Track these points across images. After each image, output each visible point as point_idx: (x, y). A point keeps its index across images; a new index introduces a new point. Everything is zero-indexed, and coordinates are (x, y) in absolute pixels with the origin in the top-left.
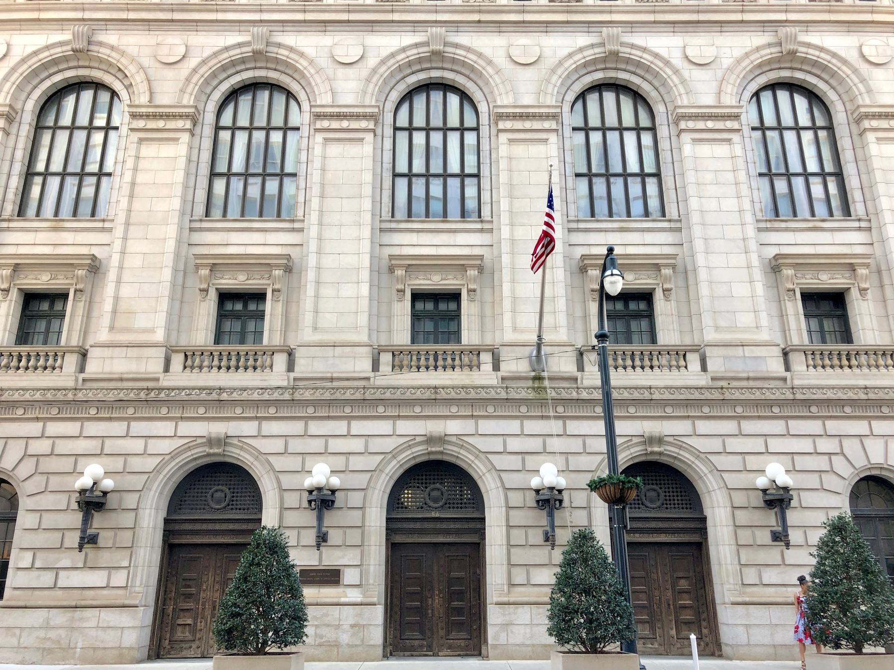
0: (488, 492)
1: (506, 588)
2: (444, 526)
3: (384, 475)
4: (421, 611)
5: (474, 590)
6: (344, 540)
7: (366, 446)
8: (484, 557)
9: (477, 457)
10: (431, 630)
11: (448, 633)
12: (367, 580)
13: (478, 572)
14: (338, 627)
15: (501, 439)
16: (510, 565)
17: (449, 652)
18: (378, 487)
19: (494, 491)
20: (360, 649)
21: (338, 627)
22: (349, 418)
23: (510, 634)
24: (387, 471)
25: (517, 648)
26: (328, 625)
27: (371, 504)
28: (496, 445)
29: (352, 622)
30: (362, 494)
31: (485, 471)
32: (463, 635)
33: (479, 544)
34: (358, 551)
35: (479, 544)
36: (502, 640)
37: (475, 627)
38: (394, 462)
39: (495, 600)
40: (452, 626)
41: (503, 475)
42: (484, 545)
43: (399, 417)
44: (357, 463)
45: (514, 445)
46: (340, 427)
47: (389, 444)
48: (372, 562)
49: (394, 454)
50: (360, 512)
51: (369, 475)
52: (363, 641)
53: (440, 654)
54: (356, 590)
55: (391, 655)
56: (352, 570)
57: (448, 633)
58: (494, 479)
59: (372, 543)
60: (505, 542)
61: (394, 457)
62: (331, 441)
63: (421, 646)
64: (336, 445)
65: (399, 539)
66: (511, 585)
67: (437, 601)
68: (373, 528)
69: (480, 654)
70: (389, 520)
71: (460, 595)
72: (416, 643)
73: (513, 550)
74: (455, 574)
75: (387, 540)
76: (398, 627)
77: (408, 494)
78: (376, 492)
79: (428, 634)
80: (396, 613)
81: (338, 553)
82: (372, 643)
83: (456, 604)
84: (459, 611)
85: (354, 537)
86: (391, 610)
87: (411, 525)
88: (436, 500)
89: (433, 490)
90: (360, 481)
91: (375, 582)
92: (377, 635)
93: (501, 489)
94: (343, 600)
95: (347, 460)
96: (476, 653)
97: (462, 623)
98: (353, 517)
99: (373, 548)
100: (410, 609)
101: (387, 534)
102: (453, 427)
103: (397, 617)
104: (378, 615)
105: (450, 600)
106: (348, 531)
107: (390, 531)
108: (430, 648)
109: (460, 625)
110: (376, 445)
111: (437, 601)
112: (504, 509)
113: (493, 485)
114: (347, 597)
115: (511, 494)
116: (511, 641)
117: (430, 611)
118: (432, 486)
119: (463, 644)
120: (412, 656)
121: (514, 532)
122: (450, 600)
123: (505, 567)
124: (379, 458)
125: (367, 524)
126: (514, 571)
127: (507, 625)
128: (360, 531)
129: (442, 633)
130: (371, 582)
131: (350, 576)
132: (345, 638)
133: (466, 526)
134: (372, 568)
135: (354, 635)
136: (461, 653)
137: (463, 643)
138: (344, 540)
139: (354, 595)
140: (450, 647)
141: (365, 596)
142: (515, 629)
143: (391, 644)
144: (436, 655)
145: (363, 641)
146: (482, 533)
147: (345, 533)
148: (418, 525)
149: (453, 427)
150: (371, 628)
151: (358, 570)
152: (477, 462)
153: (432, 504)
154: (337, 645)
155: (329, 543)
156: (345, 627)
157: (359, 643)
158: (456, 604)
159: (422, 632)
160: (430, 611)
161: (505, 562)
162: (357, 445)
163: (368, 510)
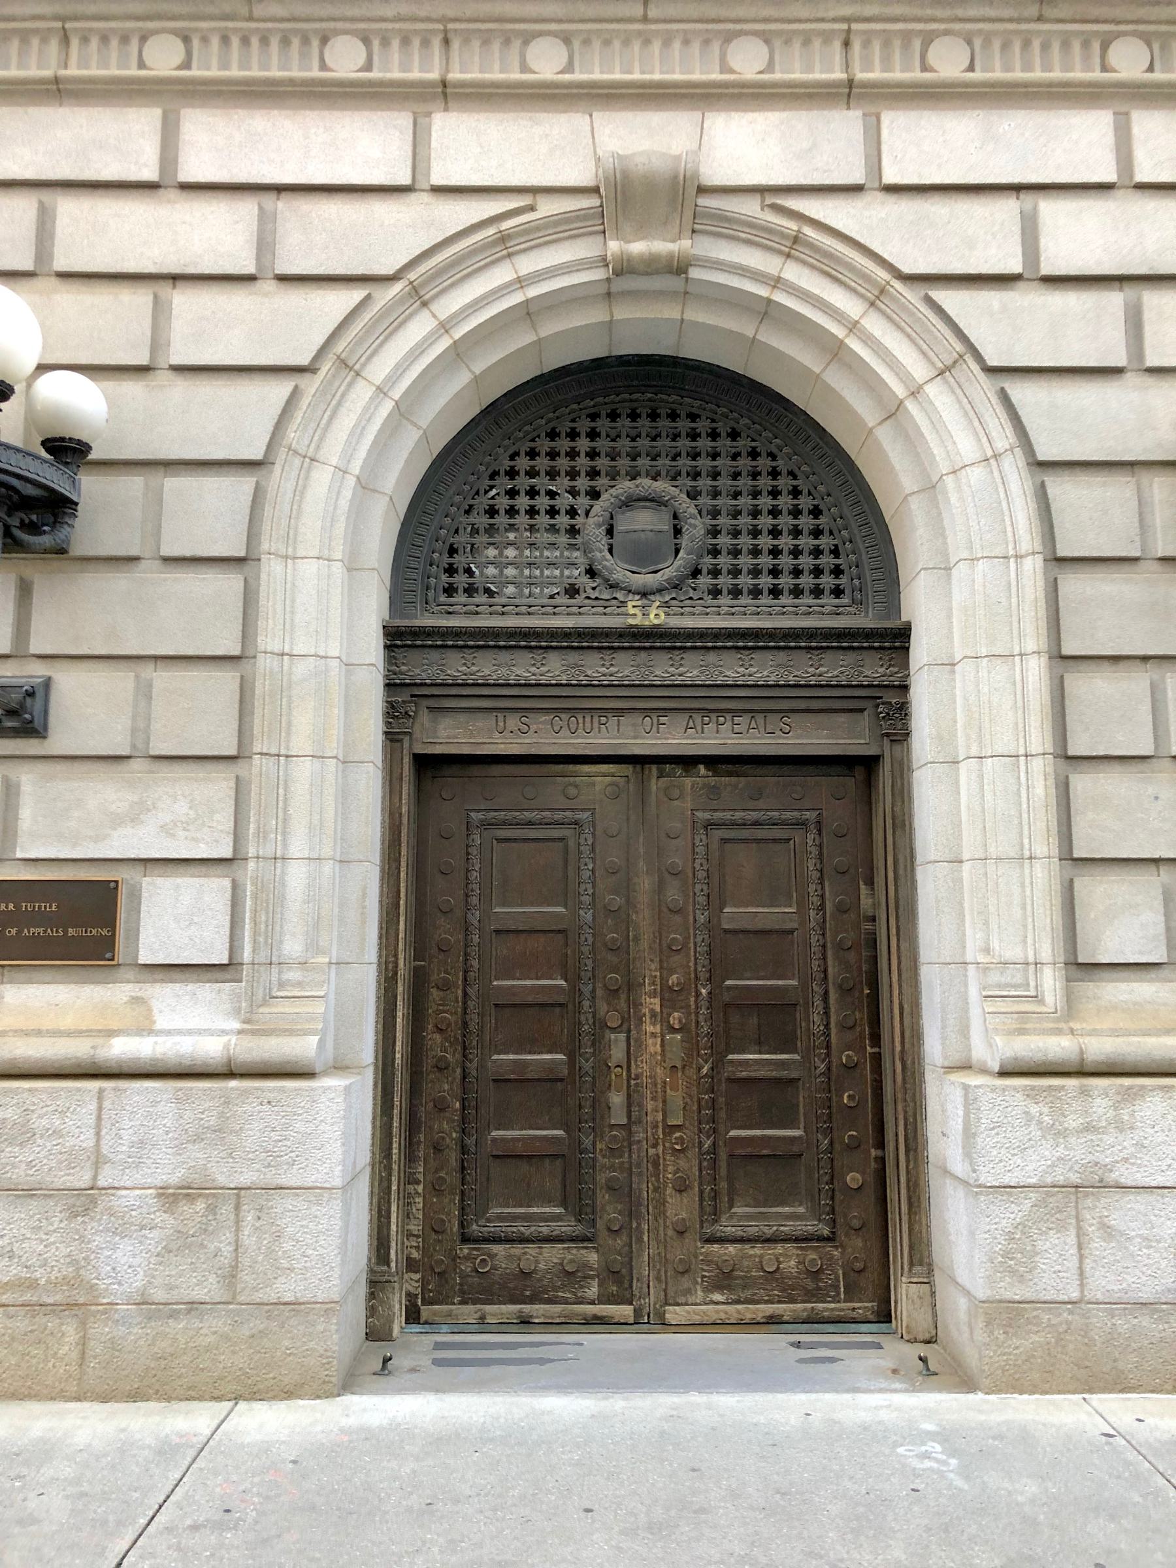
0: (931, 488)
1: (1051, 982)
2: (691, 669)
3: (362, 393)
4: (570, 1094)
5: (846, 991)
6: (141, 727)
7: (265, 244)
8: (903, 824)
9: (877, 299)
10: (624, 1193)
11: (712, 1208)
12: (269, 935)
13: (866, 901)
14: (85, 1201)
15: (1007, 209)
16: (1074, 862)
17: (718, 1306)
18: (333, 451)
19: (976, 474)
20: (213, 1325)
21: (85, 1201)
22: (175, 94)
23: (1097, 1245)
24: (380, 368)
25: (1145, 1321)
26: (29, 1192)
27: (291, 537)
28: (984, 237)
29: (169, 1172)
30: (242, 486)
31: (919, 370)
32: (795, 1216)
33: (870, 764)
34: (217, 787)
35: (870, 764)
36: (1053, 1273)
37: (853, 1179)
38: (419, 327)
39: (993, 1045)
40: (737, 1172)
41: (1023, 393)
42: (903, 770)
43: (446, 93)
44: (210, 326)
45: (1078, 236)
46: (122, 141)
47: (391, 235)
48: (298, 846)
49: (418, 281)
50: (229, 583)
51: (278, 391)
52: (231, 1276)
53: (675, 1314)
54: (206, 991)
55: (413, 1316)
56: (187, 885)
57: (712, 1208)
58: (972, 415)
59: (300, 742)
60: (1039, 739)
61: (419, 298)
62: (70, 211)
63: (572, 1276)
64: (97, 233)
65: (451, 735)
66: (1082, 968)
67: (654, 1046)
68: (301, 669)
69: (884, 1315)
70: (398, 639)
71: (775, 1020)
72: (551, 1255)
73: (1083, 783)
74: (734, 914)
75: (392, 737)
76: (451, 1177)
77: (500, 565)
78: (322, 478)
79: (611, 1213)
80: (441, 1107)
81: (104, 793)
82: (286, 1288)
83: (752, 1059)
84: (772, 1097)
85: (196, 712)
86: (414, 1090)
87: (521, 668)
88: (644, 555)
89: (629, 503)
90: (236, 419)
91: (313, 946)
92: (322, 1242)
93: (1014, 470)
94: (124, 1048)
95: (160, 312)
96: (865, 1307)
97: (784, 1158)
98: (195, 613)
99: (303, 770)
100: (515, 1082)
101: (393, 713)
102: (743, 148)
103: (447, 1129)
104: (330, 1130)
105: (723, 1042)
106: (163, 679)
107: (404, 699)
108: (619, 1283)
109: (770, 1170)
110: (316, 237)
111: (654, 1046)
112: (1033, 566)
113: (966, 447)
114: (146, 1029)
115: (1066, 492)
116: (1102, 1283)
117: (617, 1099)
118: (625, 486)
119: (791, 1265)
120: (525, 1322)
121: (1092, 690)
122: (723, 1042)
123: (1043, 876)
124: (337, 303)
125: (269, 640)
126: (1096, 891)
127: (1079, 1194)
128: (226, 680)
129: (681, 1208)
130: (293, 947)
131: (171, 919)
132: (126, 1264)
133: (805, 668)
134: (296, 877)
135: (181, 1244)
136: (783, 1309)
137: (790, 1259)
138: (141, 727)
139: (193, 1023)
140: (724, 1279)
141: (252, 1028)
142: (1125, 1213)
143: (411, 1265)
144: (650, 1320)
145: (231, 1276)
146: (890, 707)
147: (145, 692)
148: (554, 668)
149: (743, 148)
150: (282, 1204)
151: (216, 888)
152: (875, 325)
153: (619, 571)
154: (77, 1302)
155: (59, 741)
156: (127, 1199)
157: (207, 1288)
158: (752, 1059)
159: (578, 1202)
160: (617, 1099)
161: (1044, 846)
162: (216, 235)
163: (272, 570)
